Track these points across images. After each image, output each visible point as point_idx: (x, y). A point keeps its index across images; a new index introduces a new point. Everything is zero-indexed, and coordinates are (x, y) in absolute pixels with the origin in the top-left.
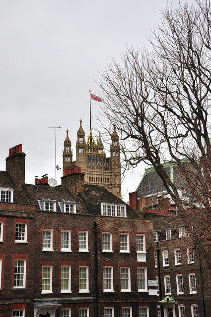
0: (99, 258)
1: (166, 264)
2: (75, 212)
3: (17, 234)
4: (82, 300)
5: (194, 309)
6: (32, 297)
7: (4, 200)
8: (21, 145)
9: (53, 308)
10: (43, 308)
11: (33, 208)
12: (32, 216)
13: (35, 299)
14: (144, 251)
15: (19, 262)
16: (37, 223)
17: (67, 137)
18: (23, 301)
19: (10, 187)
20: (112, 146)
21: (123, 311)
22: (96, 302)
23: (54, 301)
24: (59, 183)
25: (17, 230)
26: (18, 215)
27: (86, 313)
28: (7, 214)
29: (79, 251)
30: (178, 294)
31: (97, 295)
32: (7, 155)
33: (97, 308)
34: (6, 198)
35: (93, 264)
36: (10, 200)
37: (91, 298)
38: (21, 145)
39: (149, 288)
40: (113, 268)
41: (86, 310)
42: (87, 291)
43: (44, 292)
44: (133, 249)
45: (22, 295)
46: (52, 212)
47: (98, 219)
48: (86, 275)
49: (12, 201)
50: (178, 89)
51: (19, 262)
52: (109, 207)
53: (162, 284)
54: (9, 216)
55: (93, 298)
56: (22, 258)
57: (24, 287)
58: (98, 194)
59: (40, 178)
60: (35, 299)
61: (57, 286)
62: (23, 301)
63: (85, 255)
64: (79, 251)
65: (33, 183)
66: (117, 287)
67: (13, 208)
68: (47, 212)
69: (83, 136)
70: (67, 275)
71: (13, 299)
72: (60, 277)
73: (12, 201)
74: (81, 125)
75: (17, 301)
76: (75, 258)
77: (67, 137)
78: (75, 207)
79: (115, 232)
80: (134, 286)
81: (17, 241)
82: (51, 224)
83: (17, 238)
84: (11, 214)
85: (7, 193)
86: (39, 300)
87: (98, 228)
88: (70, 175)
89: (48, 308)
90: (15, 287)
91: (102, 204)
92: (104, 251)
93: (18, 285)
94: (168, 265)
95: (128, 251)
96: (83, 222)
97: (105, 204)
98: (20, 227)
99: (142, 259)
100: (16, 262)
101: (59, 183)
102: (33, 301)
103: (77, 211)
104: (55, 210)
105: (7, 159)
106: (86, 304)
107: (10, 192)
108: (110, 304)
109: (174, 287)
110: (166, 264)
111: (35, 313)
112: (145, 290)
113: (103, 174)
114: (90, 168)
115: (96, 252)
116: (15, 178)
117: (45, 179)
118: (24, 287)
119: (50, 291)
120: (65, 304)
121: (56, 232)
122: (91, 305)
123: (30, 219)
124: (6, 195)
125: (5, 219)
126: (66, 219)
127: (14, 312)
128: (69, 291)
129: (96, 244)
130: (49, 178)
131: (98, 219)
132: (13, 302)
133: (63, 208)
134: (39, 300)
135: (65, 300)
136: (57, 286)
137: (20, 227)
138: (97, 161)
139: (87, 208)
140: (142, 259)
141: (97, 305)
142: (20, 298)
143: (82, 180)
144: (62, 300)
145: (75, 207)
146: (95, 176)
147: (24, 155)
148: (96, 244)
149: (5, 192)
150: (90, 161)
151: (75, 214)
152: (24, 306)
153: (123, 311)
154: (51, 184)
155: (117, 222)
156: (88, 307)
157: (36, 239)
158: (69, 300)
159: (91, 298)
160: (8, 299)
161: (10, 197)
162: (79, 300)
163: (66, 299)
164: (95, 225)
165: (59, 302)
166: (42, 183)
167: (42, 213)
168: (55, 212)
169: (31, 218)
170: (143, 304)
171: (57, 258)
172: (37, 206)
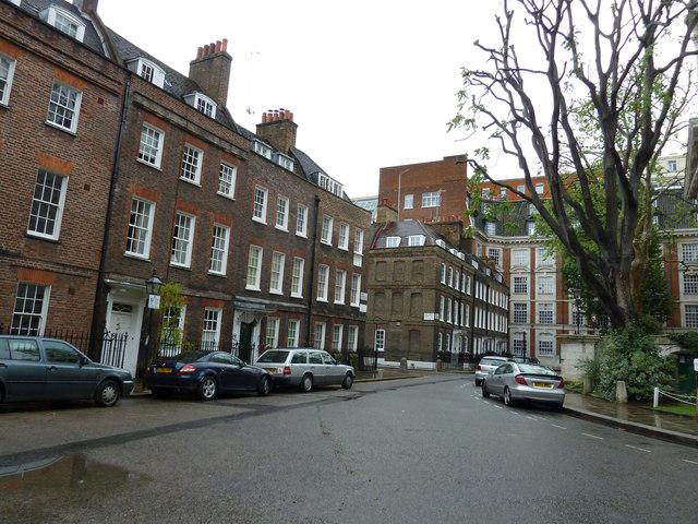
8: (225, 41)
14: (360, 253)
18: (221, 295)
20: (60, 188)
22: (308, 313)
23: (261, 303)
28: (210, 139)
32: (194, 57)
35: (309, 256)
38: (225, 41)
45: (220, 286)
48: (300, 272)
61: (265, 282)
62: (221, 295)
66: (331, 296)
71: (205, 290)
76: (288, 243)
84: (216, 141)
99: (358, 263)
105: (192, 64)
106: (296, 314)
111: (235, 318)
132: (206, 295)
134: (244, 298)
137: (43, 213)
147: (229, 59)
152: (222, 304)
162: (289, 307)
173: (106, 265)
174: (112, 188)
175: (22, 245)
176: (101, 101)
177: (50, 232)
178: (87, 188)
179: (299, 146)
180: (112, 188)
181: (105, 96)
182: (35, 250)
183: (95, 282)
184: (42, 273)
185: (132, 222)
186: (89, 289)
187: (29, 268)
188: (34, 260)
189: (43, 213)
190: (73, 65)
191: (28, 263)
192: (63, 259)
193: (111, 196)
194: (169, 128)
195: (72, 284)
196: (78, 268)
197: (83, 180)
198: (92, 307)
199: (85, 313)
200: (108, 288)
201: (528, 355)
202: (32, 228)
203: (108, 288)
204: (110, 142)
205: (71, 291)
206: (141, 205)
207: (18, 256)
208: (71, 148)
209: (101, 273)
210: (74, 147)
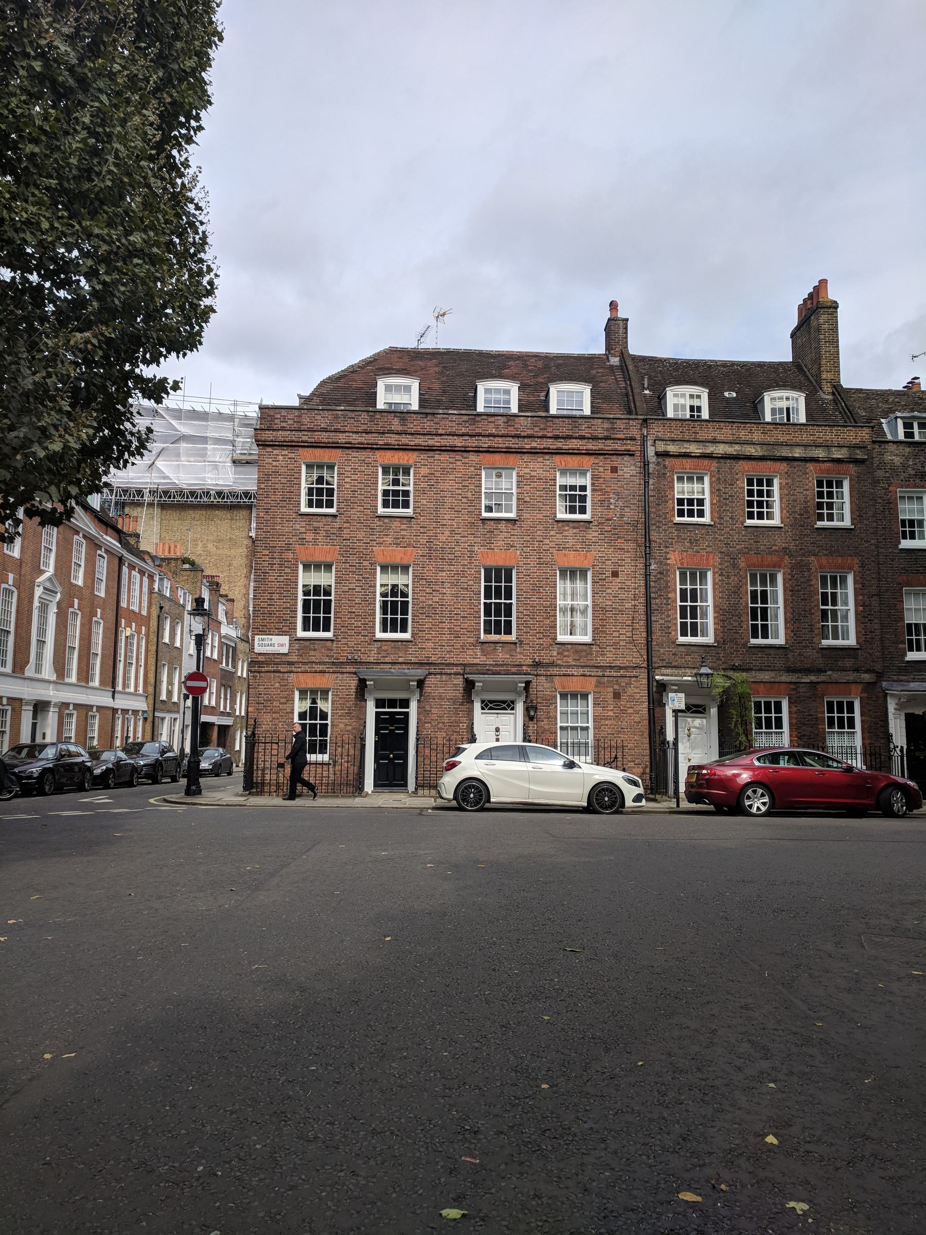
18: (852, 676)
28: (785, 452)
71: (820, 671)
83: (751, 516)
84: (798, 453)
132: (822, 678)
160: (808, 671)
173: (654, 659)
174: (647, 566)
175: (555, 653)
176: (614, 470)
177: (508, 632)
178: (615, 574)
179: (631, 353)
180: (647, 566)
181: (617, 461)
182: (568, 656)
183: (645, 681)
184: (768, 686)
185: (825, 602)
186: (638, 690)
187: (565, 675)
188: (569, 667)
189: (498, 614)
190: (405, 440)
191: (564, 671)
192: (602, 661)
193: (647, 575)
194: (714, 464)
195: (616, 687)
196: (620, 668)
197: (609, 567)
198: (645, 711)
199: (637, 719)
200: (663, 687)
201: (619, 764)
202: (755, 636)
203: (663, 687)
204: (632, 514)
205: (617, 695)
206: (834, 579)
207: (552, 664)
208: (590, 537)
209: (650, 669)
210: (592, 534)
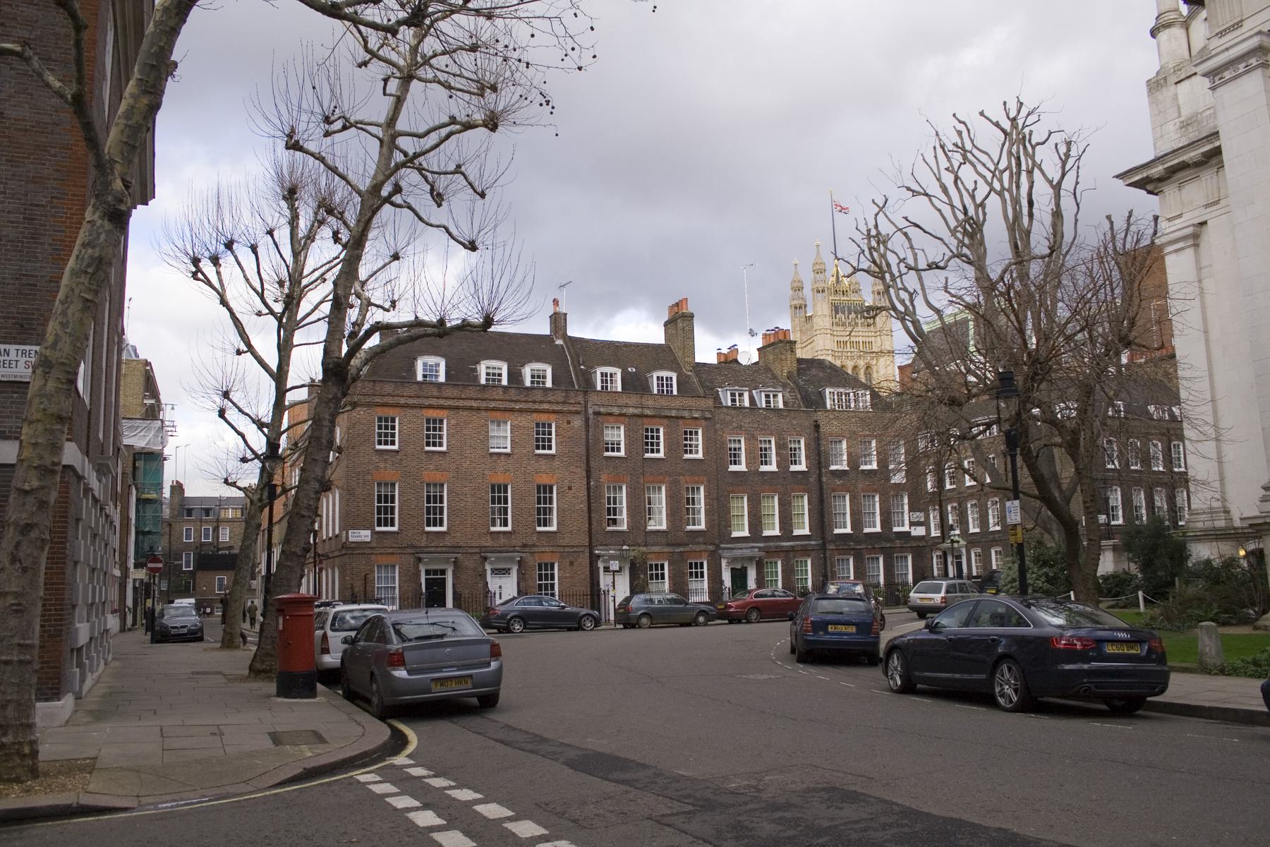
0: (824, 479)
1: (951, 484)
2: (781, 406)
3: (686, 446)
4: (797, 545)
5: (976, 556)
6: (717, 542)
7: (663, 390)
9: (751, 559)
10: (735, 560)
11: (710, 402)
12: (708, 415)
13: (722, 546)
15: (693, 488)
16: (718, 426)
17: (796, 273)
18: (703, 547)
19: (672, 370)
21: (838, 562)
23: (752, 547)
24: (755, 358)
25: (647, 437)
26: (686, 414)
27: (806, 566)
28: (667, 413)
29: (790, 470)
30: (971, 532)
31: (823, 538)
33: (825, 558)
34: (665, 389)
36: (672, 391)
37: (813, 543)
39: (912, 524)
40: (1121, 490)
41: (806, 562)
42: (806, 531)
43: (735, 534)
44: (883, 463)
45: (701, 540)
46: (742, 408)
47: (820, 416)
49: (675, 392)
50: (367, 280)
51: (693, 488)
52: (839, 395)
53: (944, 517)
54: (672, 417)
55: (818, 542)
56: (697, 482)
57: (703, 527)
58: (821, 374)
59: (725, 351)
60: (722, 546)
61: (756, 524)
63: (800, 476)
64: (790, 470)
65: (713, 360)
66: (857, 524)
67: (677, 403)
68: (734, 407)
69: (822, 271)
70: (773, 506)
72: (760, 512)
73: (675, 392)
74: (818, 252)
75: (697, 548)
76: (785, 483)
77: (796, 273)
78: (780, 395)
79: (852, 437)
80: (887, 522)
81: (687, 456)
82: (740, 427)
83: (686, 452)
84: (674, 413)
85: (667, 380)
86: (729, 546)
87: (821, 430)
88: (773, 344)
89: (743, 559)
90: (690, 528)
91: (827, 391)
92: (833, 468)
93: (694, 525)
94: (954, 486)
95: (874, 466)
96: (794, 422)
97: (832, 390)
98: (652, 431)
99: (898, 478)
100: (688, 488)
101: (755, 358)
102: (718, 547)
103: (785, 403)
104: (747, 404)
106: (805, 551)
107: (671, 378)
108: (847, 551)
109: (963, 521)
110: (951, 484)
112: (906, 528)
113: (860, 333)
114: (837, 325)
115: (820, 471)
116: (679, 354)
117: (734, 353)
118: (703, 527)
119: (746, 533)
120: (770, 552)
121: (749, 440)
122: (813, 554)
123: (709, 421)
124: (665, 382)
125: (666, 421)
126: (766, 418)
127: (691, 564)
128: (777, 532)
129: (819, 458)
130: (739, 351)
131: (820, 416)
132: (687, 549)
133: (761, 400)
134: (729, 546)
135: (770, 547)
136: (756, 524)
137: (652, 431)
138: (850, 313)
139: (802, 398)
140: (898, 478)
141: (825, 554)
142: (698, 543)
143: (793, 351)
144: (765, 547)
145: (780, 395)
146: (861, 339)
148: (819, 458)
149: (662, 378)
150: (837, 313)
151: (781, 409)
152: (705, 555)
153: (838, 562)
154: (743, 360)
155: (853, 420)
156: (809, 556)
157: (720, 454)
158: (777, 547)
159: (813, 543)
160: (679, 545)
161: (672, 386)
163: (771, 544)
164: (817, 427)
165: (760, 548)
166: (729, 362)
167: (725, 410)
168: (747, 408)
169: (706, 419)
170: (902, 549)
171: (755, 485)
172: (717, 398)
